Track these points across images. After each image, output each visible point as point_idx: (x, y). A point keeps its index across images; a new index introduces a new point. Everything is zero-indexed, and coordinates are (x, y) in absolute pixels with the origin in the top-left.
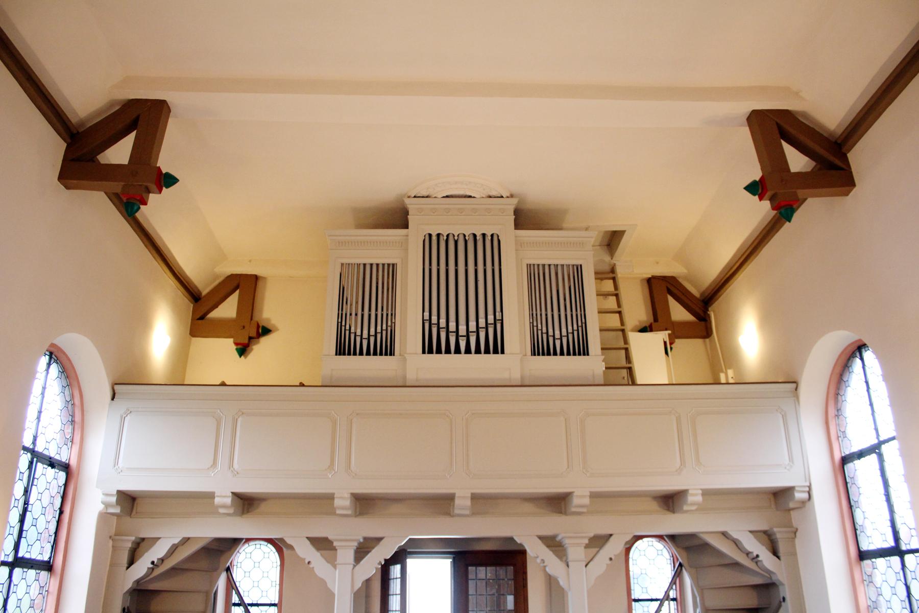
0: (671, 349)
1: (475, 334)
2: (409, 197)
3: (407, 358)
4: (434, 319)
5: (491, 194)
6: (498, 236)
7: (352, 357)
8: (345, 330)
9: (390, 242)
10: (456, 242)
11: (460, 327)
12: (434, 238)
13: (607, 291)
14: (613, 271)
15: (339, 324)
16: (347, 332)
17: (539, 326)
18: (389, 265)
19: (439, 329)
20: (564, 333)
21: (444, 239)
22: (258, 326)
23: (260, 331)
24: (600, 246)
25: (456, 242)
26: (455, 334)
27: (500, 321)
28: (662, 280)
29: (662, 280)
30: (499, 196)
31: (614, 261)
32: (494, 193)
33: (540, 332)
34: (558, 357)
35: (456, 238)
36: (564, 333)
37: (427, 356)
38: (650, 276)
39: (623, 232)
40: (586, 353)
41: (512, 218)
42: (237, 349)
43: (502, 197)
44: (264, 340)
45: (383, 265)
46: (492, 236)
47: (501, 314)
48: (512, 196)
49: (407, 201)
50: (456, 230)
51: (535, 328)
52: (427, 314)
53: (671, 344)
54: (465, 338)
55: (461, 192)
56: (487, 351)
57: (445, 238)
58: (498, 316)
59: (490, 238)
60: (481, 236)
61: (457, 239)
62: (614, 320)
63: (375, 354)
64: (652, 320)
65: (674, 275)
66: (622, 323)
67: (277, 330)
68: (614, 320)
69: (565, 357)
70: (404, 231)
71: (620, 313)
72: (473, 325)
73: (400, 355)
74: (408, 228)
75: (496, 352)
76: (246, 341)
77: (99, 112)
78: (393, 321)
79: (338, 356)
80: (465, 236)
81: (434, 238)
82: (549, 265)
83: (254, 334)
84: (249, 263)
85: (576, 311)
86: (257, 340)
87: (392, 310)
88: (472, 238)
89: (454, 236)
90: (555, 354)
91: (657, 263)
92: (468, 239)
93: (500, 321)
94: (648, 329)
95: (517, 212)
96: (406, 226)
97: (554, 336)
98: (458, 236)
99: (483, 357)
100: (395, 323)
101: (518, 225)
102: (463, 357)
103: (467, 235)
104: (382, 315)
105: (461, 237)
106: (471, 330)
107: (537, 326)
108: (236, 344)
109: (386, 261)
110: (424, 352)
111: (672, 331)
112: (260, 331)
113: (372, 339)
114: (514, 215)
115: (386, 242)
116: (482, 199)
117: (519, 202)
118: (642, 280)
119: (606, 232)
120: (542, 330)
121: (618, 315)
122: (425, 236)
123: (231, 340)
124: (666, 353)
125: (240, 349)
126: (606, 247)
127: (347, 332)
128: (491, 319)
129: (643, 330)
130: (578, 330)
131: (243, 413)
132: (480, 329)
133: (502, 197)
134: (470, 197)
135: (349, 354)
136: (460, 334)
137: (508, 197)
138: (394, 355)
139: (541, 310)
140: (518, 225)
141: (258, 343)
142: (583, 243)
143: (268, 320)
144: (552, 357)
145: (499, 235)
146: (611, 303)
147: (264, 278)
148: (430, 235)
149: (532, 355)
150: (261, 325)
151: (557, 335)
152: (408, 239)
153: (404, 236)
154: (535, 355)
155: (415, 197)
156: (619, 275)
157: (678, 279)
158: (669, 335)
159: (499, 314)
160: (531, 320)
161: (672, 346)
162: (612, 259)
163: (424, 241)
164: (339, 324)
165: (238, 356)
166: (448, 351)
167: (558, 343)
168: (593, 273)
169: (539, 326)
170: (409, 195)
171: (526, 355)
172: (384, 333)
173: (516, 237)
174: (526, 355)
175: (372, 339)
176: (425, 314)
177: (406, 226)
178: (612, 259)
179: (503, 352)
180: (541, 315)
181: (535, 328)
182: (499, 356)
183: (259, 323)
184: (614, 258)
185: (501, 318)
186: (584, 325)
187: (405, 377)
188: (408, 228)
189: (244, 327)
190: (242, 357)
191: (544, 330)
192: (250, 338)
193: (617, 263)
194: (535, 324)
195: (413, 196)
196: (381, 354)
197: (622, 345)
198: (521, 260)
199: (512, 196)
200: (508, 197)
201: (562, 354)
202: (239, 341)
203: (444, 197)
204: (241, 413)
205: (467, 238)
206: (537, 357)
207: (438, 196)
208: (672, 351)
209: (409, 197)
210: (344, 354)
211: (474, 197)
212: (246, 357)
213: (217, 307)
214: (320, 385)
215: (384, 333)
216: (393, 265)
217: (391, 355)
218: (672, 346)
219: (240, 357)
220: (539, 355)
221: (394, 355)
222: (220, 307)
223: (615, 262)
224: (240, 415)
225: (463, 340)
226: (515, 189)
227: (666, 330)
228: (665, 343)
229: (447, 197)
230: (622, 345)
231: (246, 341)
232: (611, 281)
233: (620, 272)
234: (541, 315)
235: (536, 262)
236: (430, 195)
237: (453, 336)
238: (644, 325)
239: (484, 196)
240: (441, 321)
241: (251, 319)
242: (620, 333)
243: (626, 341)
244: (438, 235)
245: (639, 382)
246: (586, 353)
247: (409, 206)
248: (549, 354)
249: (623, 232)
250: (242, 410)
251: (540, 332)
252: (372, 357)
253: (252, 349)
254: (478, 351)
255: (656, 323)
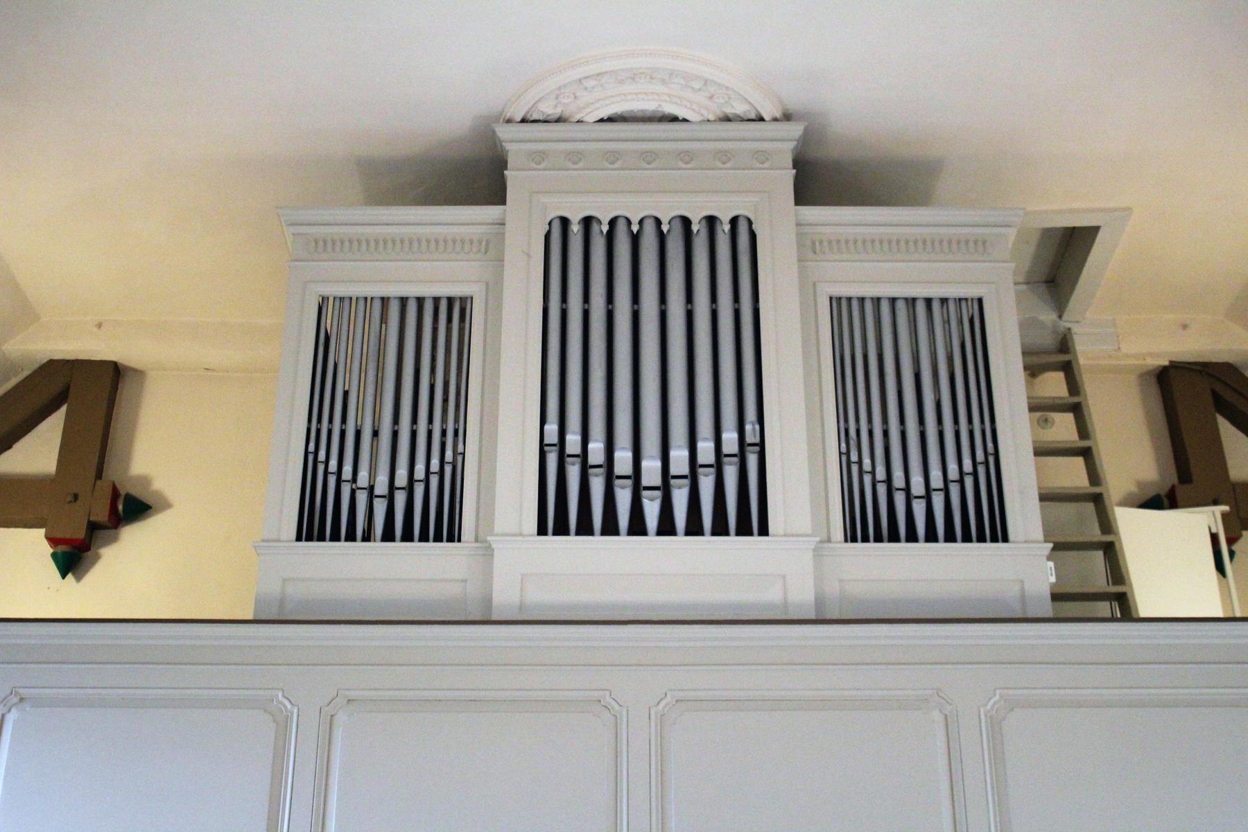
0: (1232, 554)
1: (686, 482)
2: (509, 121)
3: (494, 546)
4: (573, 441)
5: (729, 111)
6: (750, 222)
7: (343, 545)
8: (326, 473)
9: (454, 241)
10: (635, 240)
11: (645, 464)
12: (575, 228)
13: (1049, 398)
14: (1064, 344)
15: (311, 458)
16: (332, 480)
17: (867, 462)
18: (450, 300)
19: (585, 468)
20: (936, 480)
21: (602, 232)
22: (115, 493)
23: (120, 507)
24: (1027, 283)
25: (635, 240)
26: (629, 482)
27: (757, 449)
28: (1201, 372)
29: (1201, 372)
30: (753, 116)
31: (1064, 324)
32: (739, 109)
33: (867, 479)
34: (922, 547)
35: (635, 228)
36: (936, 480)
37: (551, 540)
38: (1166, 363)
39: (1093, 231)
40: (998, 532)
41: (788, 176)
42: (54, 556)
43: (762, 119)
44: (133, 536)
45: (436, 300)
46: (734, 221)
47: (757, 427)
48: (787, 117)
49: (503, 132)
50: (635, 208)
51: (855, 468)
52: (552, 428)
53: (1231, 541)
54: (658, 493)
55: (649, 106)
56: (720, 529)
57: (605, 228)
58: (751, 435)
59: (727, 227)
60: (704, 222)
61: (638, 232)
62: (1072, 474)
63: (407, 537)
64: (1173, 479)
65: (1230, 361)
66: (1094, 476)
67: (166, 505)
68: (1072, 474)
69: (941, 547)
70: (492, 212)
71: (1086, 454)
72: (679, 456)
73: (477, 540)
74: (505, 204)
75: (744, 529)
76: (81, 534)
77: (136, 407)
78: (460, 449)
79: (303, 544)
80: (658, 222)
81: (575, 228)
82: (893, 301)
83: (101, 515)
84: (95, 330)
85: (970, 421)
86: (113, 531)
87: (456, 420)
88: (678, 226)
89: (629, 222)
90: (912, 537)
91: (1185, 327)
92: (669, 231)
93: (757, 449)
94: (1166, 501)
95: (801, 164)
96: (498, 196)
97: (907, 490)
98: (641, 222)
99: (707, 544)
100: (463, 454)
101: (803, 196)
102: (652, 543)
103: (665, 221)
104: (430, 433)
105: (649, 228)
106: (674, 470)
107: (860, 462)
108: (52, 541)
109: (444, 291)
110: (542, 531)
111: (1231, 507)
112: (120, 507)
113: (400, 499)
114: (794, 167)
115: (445, 241)
116: (709, 126)
117: (806, 131)
118: (1144, 376)
119: (1047, 233)
120: (873, 473)
121: (1080, 461)
122: (550, 224)
123: (42, 531)
124: (1220, 567)
125: (64, 553)
126: (1043, 288)
127: (332, 480)
128: (730, 439)
129: (1154, 503)
130: (975, 474)
131: (22, 700)
132: (701, 470)
133: (762, 119)
134: (674, 119)
135: (335, 537)
136: (645, 481)
137: (775, 120)
138: (459, 540)
139: (870, 420)
140: (803, 196)
141: (114, 539)
142: (984, 243)
143: (145, 481)
144: (903, 547)
145: (752, 219)
146: (1063, 428)
147: (139, 374)
148: (565, 222)
149: (846, 541)
150: (123, 493)
151: (918, 487)
152: (503, 234)
153: (493, 224)
154: (854, 540)
155: (523, 121)
156: (1082, 361)
157: (1243, 371)
158: (1225, 516)
159: (754, 429)
160: (843, 445)
161: (1234, 547)
162: (1060, 317)
163: (547, 237)
164: (311, 458)
165: (57, 574)
166: (610, 528)
167: (919, 508)
168: (1019, 351)
169: (867, 462)
170: (508, 116)
171: (829, 541)
172: (434, 481)
173: (798, 225)
174: (829, 541)
175: (400, 499)
176: (546, 427)
177: (498, 196)
178: (1060, 317)
179: (764, 531)
180: (871, 433)
181: (855, 468)
182: (756, 540)
183: (118, 486)
184: (1065, 317)
185: (757, 440)
186: (991, 459)
187: (487, 601)
188: (505, 204)
189: (76, 497)
190: (70, 576)
191: (881, 473)
192: (93, 527)
193: (1075, 329)
194: (854, 458)
195: (519, 120)
196: (424, 538)
197: (1095, 534)
198: (814, 284)
199: (787, 117)
200: (775, 120)
201: (931, 537)
202: (59, 535)
203: (602, 120)
204: (15, 700)
205: (665, 228)
206: (860, 545)
207: (587, 119)
208: (1236, 558)
209: (509, 121)
210: (321, 538)
211: (685, 120)
212: (78, 578)
213: (10, 447)
214: (250, 617)
215: (434, 481)
216: (463, 300)
217: (451, 539)
218: (1234, 547)
219: (64, 576)
220: (865, 539)
221: (459, 540)
222: (18, 446)
223: (1068, 325)
224: (14, 705)
225: (652, 500)
226: (795, 98)
227: (1215, 502)
228: (1214, 538)
229: (611, 120)
230: (1095, 534)
231: (81, 534)
232: (1059, 376)
233: (1085, 352)
234: (871, 433)
235: (854, 291)
236: (566, 114)
237: (623, 487)
238: (1152, 493)
239: (711, 117)
240: (591, 446)
241: (99, 474)
242: (1090, 507)
243: (1107, 525)
244: (587, 222)
245: (1145, 605)
246: (998, 532)
247: (508, 146)
248: (894, 538)
249: (1093, 231)
250: (21, 691)
251: (867, 479)
252: (398, 547)
253: (97, 558)
254: (694, 528)
255: (1186, 487)
